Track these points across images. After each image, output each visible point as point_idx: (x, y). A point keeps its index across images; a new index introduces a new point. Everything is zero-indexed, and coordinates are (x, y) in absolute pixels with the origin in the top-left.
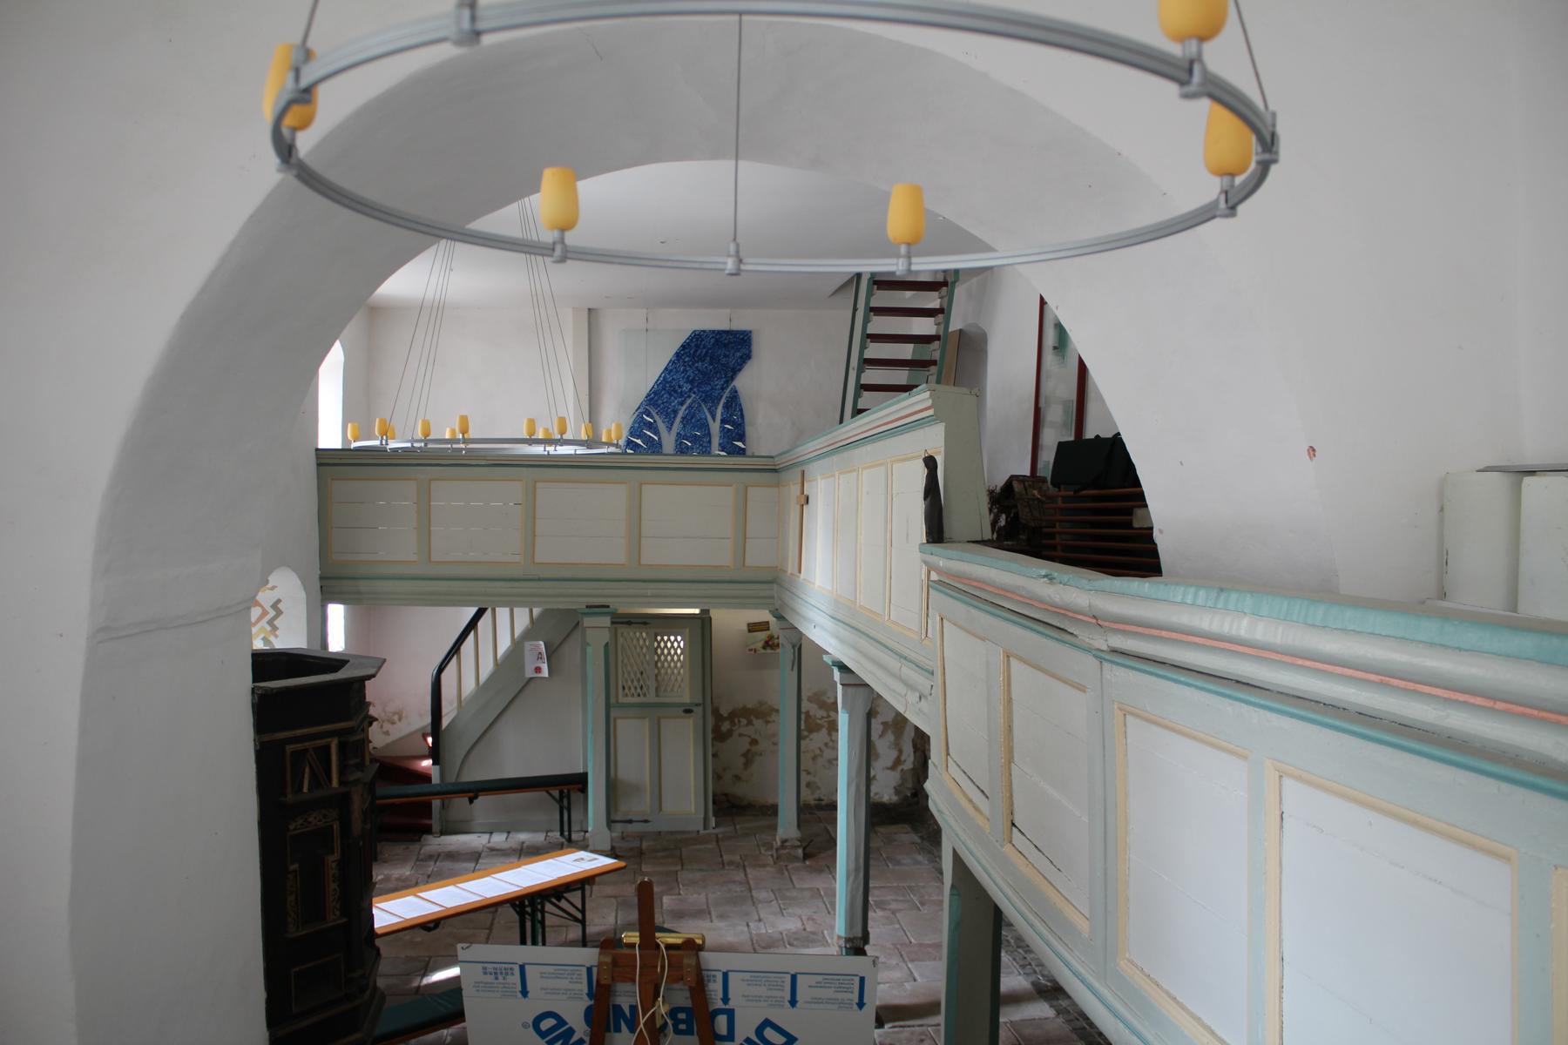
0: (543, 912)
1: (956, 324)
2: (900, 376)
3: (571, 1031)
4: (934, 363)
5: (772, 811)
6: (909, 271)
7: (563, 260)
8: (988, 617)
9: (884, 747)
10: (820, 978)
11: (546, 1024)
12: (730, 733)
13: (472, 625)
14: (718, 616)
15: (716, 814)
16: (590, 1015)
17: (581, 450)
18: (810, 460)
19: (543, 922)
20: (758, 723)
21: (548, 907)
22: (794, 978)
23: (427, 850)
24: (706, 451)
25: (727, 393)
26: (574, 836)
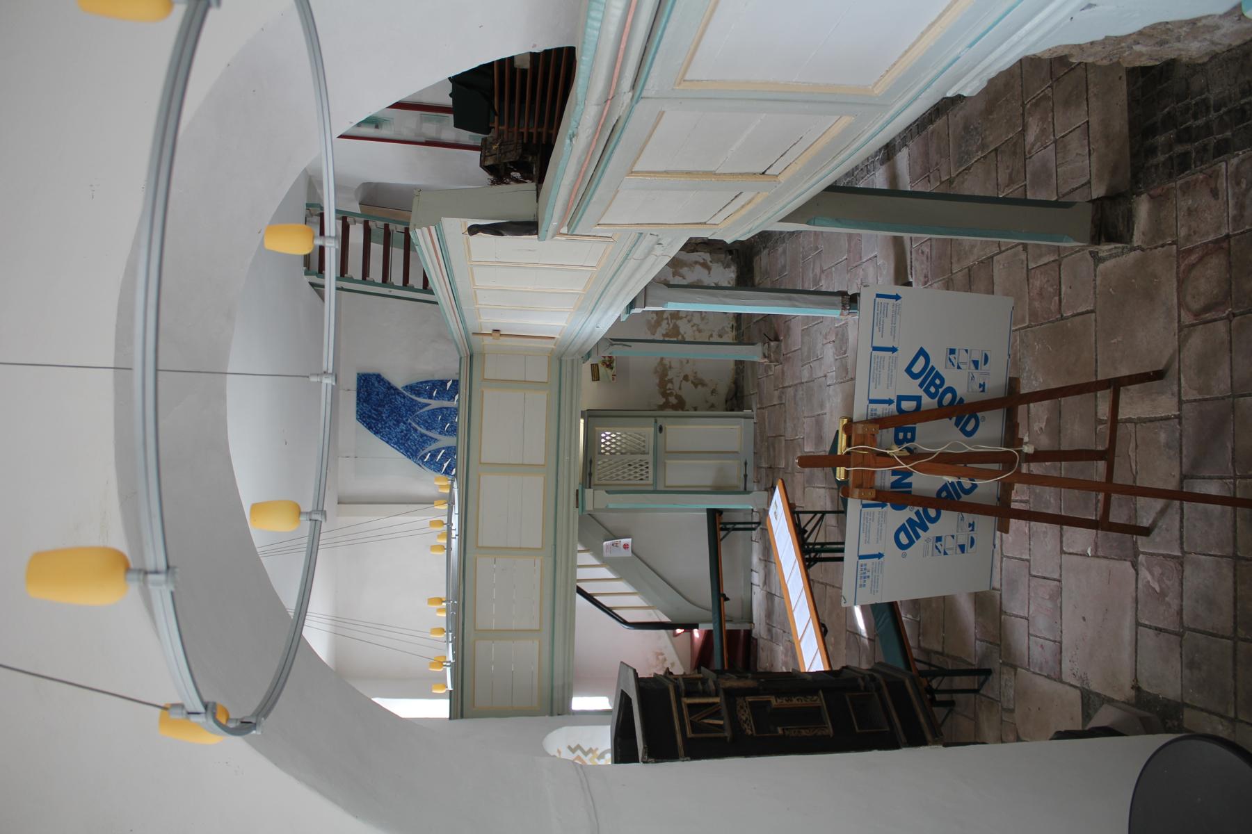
0: (815, 544)
1: (356, 208)
2: (397, 254)
3: (910, 521)
4: (386, 226)
5: (739, 364)
6: (336, 237)
7: (324, 513)
8: (600, 186)
9: (692, 276)
10: (876, 329)
11: (903, 539)
12: (678, 397)
13: (590, 597)
14: (587, 403)
15: (741, 410)
16: (898, 506)
17: (456, 510)
18: (465, 328)
19: (822, 544)
20: (671, 375)
21: (811, 540)
22: (875, 349)
23: (764, 634)
24: (455, 411)
25: (407, 394)
26: (756, 519)
